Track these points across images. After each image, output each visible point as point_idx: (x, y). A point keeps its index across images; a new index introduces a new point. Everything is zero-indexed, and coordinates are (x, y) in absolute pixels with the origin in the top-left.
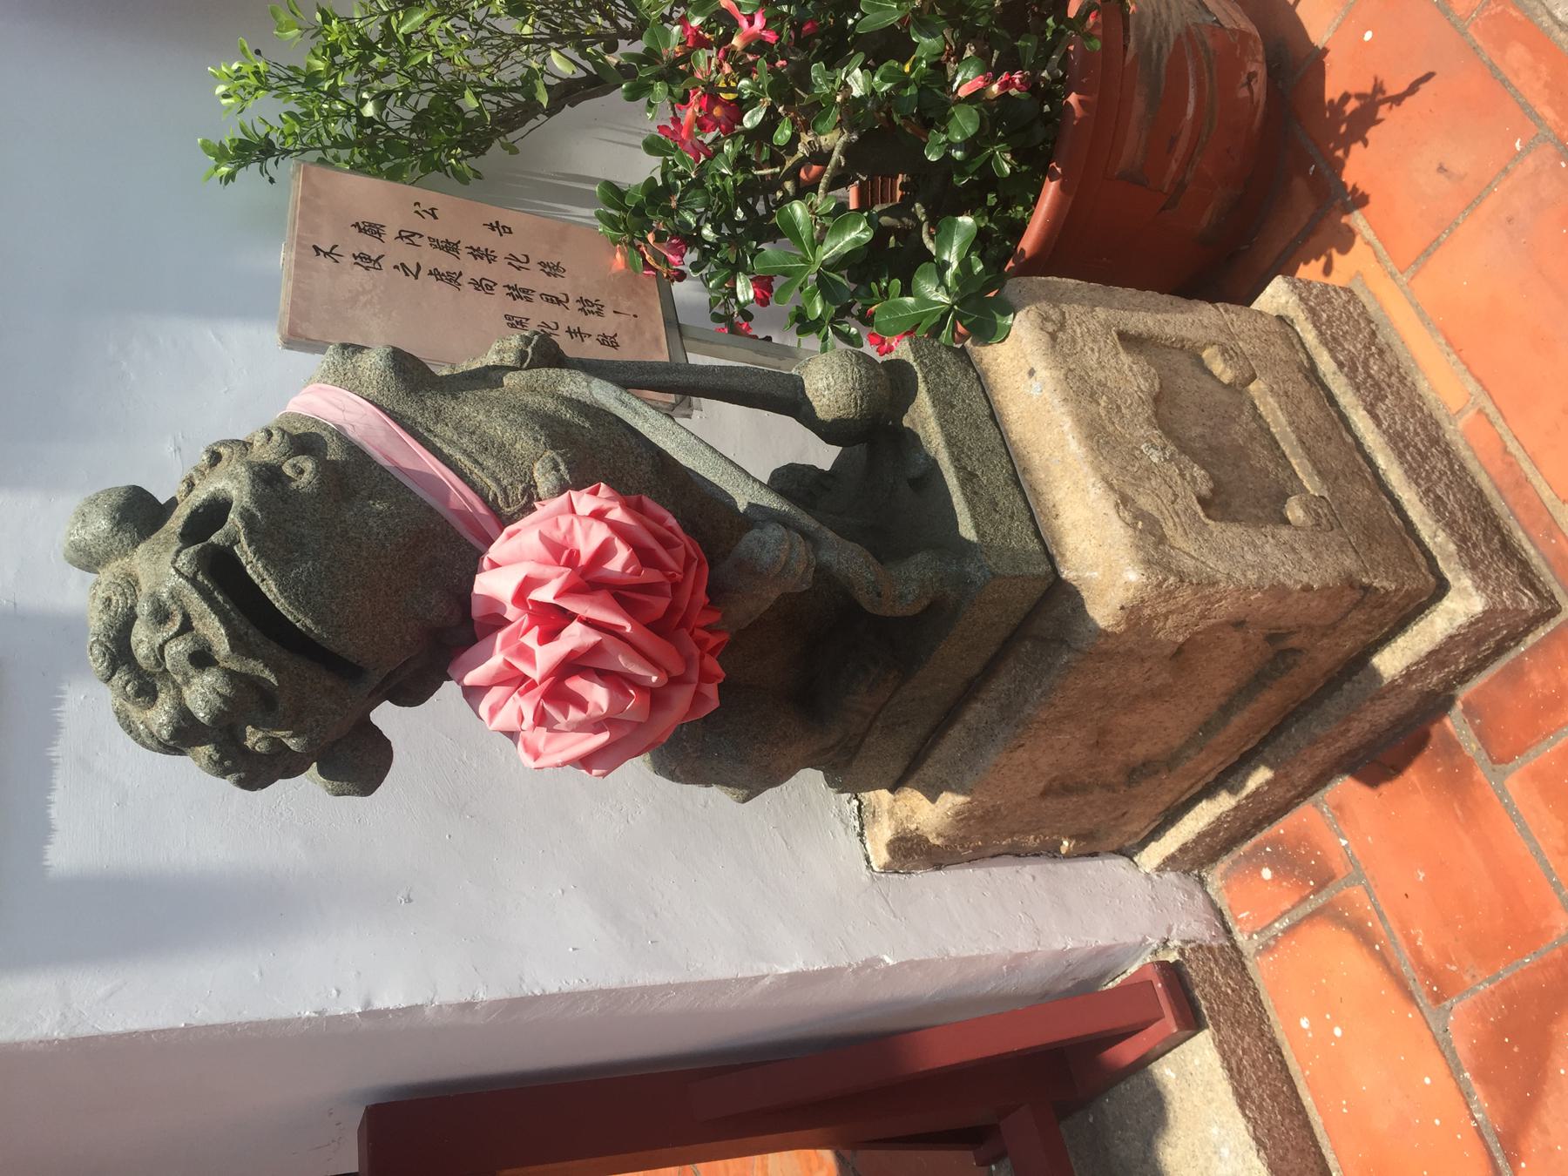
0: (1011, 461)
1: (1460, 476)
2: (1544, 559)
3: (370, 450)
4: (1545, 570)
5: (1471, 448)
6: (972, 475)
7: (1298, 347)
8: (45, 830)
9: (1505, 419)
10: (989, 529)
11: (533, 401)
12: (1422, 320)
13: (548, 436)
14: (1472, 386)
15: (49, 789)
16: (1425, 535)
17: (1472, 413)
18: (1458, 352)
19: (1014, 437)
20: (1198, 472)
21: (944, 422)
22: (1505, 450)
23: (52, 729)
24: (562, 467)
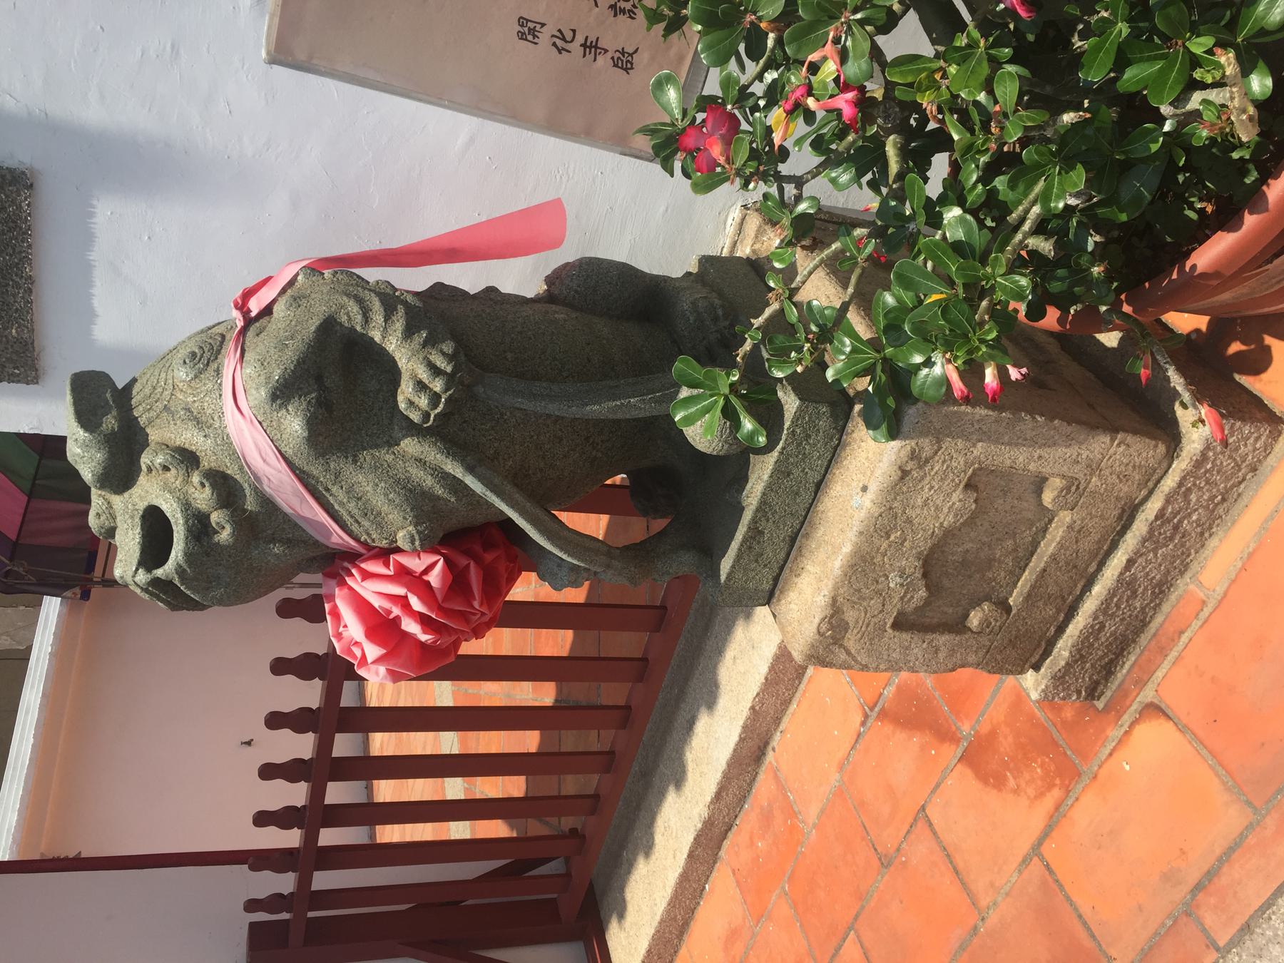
0: (803, 523)
1: (1161, 589)
2: (1123, 681)
3: (280, 501)
4: (1117, 683)
5: (1178, 601)
6: (761, 533)
7: (1151, 484)
8: (91, 315)
9: (1201, 627)
10: (739, 575)
11: (417, 474)
12: (1266, 521)
13: (415, 517)
14: (1220, 590)
15: (89, 284)
16: (1060, 644)
17: (1201, 595)
18: (1244, 568)
19: (821, 507)
20: (922, 593)
21: (769, 487)
22: (1182, 632)
23: (88, 238)
24: (417, 543)
